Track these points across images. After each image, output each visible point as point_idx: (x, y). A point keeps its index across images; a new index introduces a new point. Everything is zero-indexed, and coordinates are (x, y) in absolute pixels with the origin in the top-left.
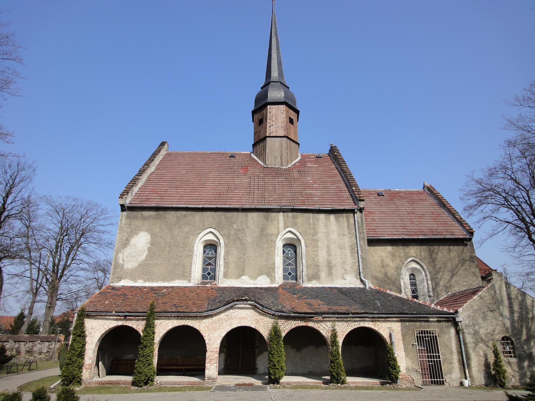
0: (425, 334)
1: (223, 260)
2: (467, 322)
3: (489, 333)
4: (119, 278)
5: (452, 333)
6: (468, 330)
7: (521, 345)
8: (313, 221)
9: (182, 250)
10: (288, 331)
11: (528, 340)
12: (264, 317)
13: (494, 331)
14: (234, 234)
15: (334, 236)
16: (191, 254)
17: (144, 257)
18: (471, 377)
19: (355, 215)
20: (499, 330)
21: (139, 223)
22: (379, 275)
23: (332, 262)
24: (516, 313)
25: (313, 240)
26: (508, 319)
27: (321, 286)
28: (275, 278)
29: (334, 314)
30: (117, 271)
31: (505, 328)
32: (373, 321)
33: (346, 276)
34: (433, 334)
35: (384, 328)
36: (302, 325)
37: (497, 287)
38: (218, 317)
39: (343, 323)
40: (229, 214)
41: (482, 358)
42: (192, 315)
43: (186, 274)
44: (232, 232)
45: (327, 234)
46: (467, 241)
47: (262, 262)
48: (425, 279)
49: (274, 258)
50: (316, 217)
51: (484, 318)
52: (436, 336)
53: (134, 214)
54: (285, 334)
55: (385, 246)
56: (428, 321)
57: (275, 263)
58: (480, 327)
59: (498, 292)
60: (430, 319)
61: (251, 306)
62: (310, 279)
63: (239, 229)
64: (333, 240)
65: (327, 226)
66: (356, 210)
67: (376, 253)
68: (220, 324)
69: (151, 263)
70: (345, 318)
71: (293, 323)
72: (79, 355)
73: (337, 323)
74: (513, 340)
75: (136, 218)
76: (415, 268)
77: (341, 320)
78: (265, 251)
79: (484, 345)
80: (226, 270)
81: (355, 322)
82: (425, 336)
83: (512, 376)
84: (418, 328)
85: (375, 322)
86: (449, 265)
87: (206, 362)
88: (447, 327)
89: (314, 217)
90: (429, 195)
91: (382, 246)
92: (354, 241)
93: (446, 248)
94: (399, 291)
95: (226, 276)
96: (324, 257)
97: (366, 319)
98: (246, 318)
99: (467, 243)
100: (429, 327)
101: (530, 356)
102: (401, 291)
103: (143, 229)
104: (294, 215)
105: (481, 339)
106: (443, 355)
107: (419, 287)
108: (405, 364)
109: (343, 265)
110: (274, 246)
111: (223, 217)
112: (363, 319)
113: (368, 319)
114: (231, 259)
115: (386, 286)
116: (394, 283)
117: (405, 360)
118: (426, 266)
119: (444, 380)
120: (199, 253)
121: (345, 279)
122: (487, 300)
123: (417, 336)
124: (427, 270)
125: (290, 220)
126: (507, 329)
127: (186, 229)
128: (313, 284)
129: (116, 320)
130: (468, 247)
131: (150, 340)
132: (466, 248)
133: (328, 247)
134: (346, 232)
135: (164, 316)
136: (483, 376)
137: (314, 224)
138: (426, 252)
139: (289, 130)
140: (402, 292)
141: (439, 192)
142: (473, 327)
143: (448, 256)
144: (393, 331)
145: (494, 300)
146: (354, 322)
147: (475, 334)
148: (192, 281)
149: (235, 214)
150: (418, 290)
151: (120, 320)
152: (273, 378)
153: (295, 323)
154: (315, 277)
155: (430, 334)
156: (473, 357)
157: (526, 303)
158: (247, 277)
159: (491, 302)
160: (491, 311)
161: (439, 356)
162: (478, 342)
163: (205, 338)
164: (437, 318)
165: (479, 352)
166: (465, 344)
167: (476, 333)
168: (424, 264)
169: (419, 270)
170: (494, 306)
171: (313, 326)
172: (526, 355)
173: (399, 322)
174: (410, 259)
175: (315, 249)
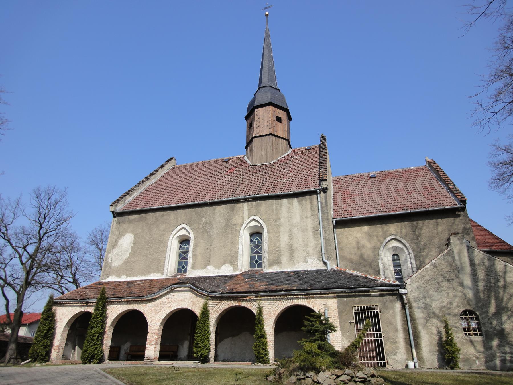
0: (364, 310)
1: (192, 252)
2: (416, 295)
3: (444, 307)
4: (107, 275)
5: (398, 308)
6: (418, 304)
7: (489, 319)
8: (276, 207)
9: (158, 246)
10: (221, 311)
11: (498, 313)
12: (200, 299)
13: (451, 303)
14: (203, 228)
15: (296, 220)
16: (165, 249)
17: (127, 255)
18: (420, 358)
19: (319, 195)
20: (458, 303)
21: (125, 226)
22: (354, 258)
23: (293, 245)
24: (482, 281)
25: (275, 226)
26: (470, 289)
27: (282, 270)
28: (238, 266)
29: (266, 292)
30: (106, 269)
31: (466, 300)
32: (307, 298)
33: (308, 259)
34: (374, 309)
35: (319, 305)
36: (234, 305)
37: (456, 251)
38: (160, 300)
39: (275, 301)
40: (199, 210)
41: (435, 337)
42: (138, 300)
43: (160, 268)
44: (201, 226)
45: (290, 218)
46: (459, 211)
47: (226, 251)
48: (409, 258)
49: (237, 247)
50: (279, 203)
51: (438, 290)
52: (377, 312)
53: (123, 219)
54: (218, 315)
55: (362, 226)
56: (369, 296)
57: (238, 252)
58: (432, 300)
59: (457, 258)
60: (371, 293)
61: (189, 289)
62: (271, 265)
63: (207, 223)
64: (295, 223)
65: (289, 211)
66: (318, 191)
67: (350, 235)
68: (161, 307)
69: (133, 260)
70: (278, 296)
71: (226, 303)
72: (44, 336)
73: (263, 302)
74: (478, 314)
75: (124, 222)
76: (397, 247)
77: (273, 299)
78: (229, 241)
79: (438, 321)
80: (194, 261)
81: (288, 300)
82: (365, 313)
83: (476, 358)
84: (357, 304)
85: (310, 299)
86: (436, 241)
87: (147, 343)
88: (391, 301)
89: (277, 203)
90: (430, 170)
91: (358, 227)
92: (317, 223)
93: (433, 221)
94: (377, 273)
95: (193, 267)
96: (285, 242)
97: (300, 296)
98: (184, 300)
99: (460, 213)
100: (369, 303)
101: (502, 334)
102: (379, 273)
103: (128, 231)
104: (258, 203)
105: (434, 313)
106: (386, 334)
107: (403, 268)
108: (341, 344)
109: (305, 248)
110: (238, 235)
111: (194, 213)
112: (297, 296)
113: (302, 296)
114: (199, 250)
115: (362, 268)
116: (370, 264)
117: (340, 339)
118: (409, 244)
119: (386, 361)
120: (173, 248)
121: (307, 262)
122: (443, 268)
123: (355, 313)
124: (410, 248)
125: (254, 209)
126: (468, 302)
127: (163, 227)
128: (274, 269)
129: (81, 306)
130: (461, 218)
131: (96, 322)
132: (458, 220)
133: (290, 231)
134: (309, 214)
135: (116, 301)
136: (436, 357)
137: (276, 210)
138: (408, 228)
139: (275, 128)
140: (380, 274)
141: (439, 165)
142: (423, 300)
143: (435, 231)
144: (328, 308)
145: (453, 268)
146: (287, 300)
147: (426, 308)
148: (165, 273)
149: (204, 209)
150: (402, 271)
151: (84, 306)
152: (196, 356)
153: (228, 303)
154: (277, 262)
155: (371, 309)
156: (424, 335)
157: (495, 269)
158: (212, 267)
159: (447, 270)
160: (448, 280)
161: (380, 334)
162: (430, 318)
163: (148, 321)
164: (379, 291)
165: (431, 329)
166: (413, 320)
167: (427, 307)
168: (406, 242)
169: (402, 249)
170: (452, 275)
171: (245, 306)
172: (495, 332)
173: (336, 298)
174: (388, 239)
175: (277, 235)
